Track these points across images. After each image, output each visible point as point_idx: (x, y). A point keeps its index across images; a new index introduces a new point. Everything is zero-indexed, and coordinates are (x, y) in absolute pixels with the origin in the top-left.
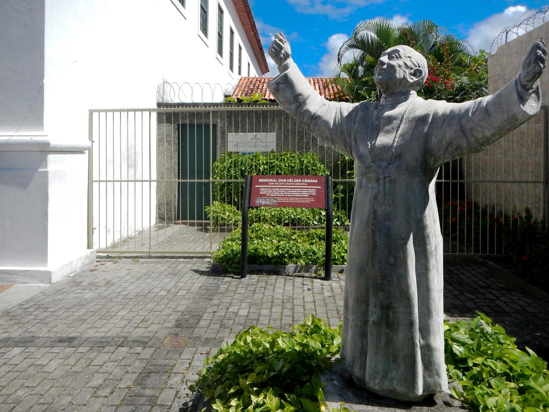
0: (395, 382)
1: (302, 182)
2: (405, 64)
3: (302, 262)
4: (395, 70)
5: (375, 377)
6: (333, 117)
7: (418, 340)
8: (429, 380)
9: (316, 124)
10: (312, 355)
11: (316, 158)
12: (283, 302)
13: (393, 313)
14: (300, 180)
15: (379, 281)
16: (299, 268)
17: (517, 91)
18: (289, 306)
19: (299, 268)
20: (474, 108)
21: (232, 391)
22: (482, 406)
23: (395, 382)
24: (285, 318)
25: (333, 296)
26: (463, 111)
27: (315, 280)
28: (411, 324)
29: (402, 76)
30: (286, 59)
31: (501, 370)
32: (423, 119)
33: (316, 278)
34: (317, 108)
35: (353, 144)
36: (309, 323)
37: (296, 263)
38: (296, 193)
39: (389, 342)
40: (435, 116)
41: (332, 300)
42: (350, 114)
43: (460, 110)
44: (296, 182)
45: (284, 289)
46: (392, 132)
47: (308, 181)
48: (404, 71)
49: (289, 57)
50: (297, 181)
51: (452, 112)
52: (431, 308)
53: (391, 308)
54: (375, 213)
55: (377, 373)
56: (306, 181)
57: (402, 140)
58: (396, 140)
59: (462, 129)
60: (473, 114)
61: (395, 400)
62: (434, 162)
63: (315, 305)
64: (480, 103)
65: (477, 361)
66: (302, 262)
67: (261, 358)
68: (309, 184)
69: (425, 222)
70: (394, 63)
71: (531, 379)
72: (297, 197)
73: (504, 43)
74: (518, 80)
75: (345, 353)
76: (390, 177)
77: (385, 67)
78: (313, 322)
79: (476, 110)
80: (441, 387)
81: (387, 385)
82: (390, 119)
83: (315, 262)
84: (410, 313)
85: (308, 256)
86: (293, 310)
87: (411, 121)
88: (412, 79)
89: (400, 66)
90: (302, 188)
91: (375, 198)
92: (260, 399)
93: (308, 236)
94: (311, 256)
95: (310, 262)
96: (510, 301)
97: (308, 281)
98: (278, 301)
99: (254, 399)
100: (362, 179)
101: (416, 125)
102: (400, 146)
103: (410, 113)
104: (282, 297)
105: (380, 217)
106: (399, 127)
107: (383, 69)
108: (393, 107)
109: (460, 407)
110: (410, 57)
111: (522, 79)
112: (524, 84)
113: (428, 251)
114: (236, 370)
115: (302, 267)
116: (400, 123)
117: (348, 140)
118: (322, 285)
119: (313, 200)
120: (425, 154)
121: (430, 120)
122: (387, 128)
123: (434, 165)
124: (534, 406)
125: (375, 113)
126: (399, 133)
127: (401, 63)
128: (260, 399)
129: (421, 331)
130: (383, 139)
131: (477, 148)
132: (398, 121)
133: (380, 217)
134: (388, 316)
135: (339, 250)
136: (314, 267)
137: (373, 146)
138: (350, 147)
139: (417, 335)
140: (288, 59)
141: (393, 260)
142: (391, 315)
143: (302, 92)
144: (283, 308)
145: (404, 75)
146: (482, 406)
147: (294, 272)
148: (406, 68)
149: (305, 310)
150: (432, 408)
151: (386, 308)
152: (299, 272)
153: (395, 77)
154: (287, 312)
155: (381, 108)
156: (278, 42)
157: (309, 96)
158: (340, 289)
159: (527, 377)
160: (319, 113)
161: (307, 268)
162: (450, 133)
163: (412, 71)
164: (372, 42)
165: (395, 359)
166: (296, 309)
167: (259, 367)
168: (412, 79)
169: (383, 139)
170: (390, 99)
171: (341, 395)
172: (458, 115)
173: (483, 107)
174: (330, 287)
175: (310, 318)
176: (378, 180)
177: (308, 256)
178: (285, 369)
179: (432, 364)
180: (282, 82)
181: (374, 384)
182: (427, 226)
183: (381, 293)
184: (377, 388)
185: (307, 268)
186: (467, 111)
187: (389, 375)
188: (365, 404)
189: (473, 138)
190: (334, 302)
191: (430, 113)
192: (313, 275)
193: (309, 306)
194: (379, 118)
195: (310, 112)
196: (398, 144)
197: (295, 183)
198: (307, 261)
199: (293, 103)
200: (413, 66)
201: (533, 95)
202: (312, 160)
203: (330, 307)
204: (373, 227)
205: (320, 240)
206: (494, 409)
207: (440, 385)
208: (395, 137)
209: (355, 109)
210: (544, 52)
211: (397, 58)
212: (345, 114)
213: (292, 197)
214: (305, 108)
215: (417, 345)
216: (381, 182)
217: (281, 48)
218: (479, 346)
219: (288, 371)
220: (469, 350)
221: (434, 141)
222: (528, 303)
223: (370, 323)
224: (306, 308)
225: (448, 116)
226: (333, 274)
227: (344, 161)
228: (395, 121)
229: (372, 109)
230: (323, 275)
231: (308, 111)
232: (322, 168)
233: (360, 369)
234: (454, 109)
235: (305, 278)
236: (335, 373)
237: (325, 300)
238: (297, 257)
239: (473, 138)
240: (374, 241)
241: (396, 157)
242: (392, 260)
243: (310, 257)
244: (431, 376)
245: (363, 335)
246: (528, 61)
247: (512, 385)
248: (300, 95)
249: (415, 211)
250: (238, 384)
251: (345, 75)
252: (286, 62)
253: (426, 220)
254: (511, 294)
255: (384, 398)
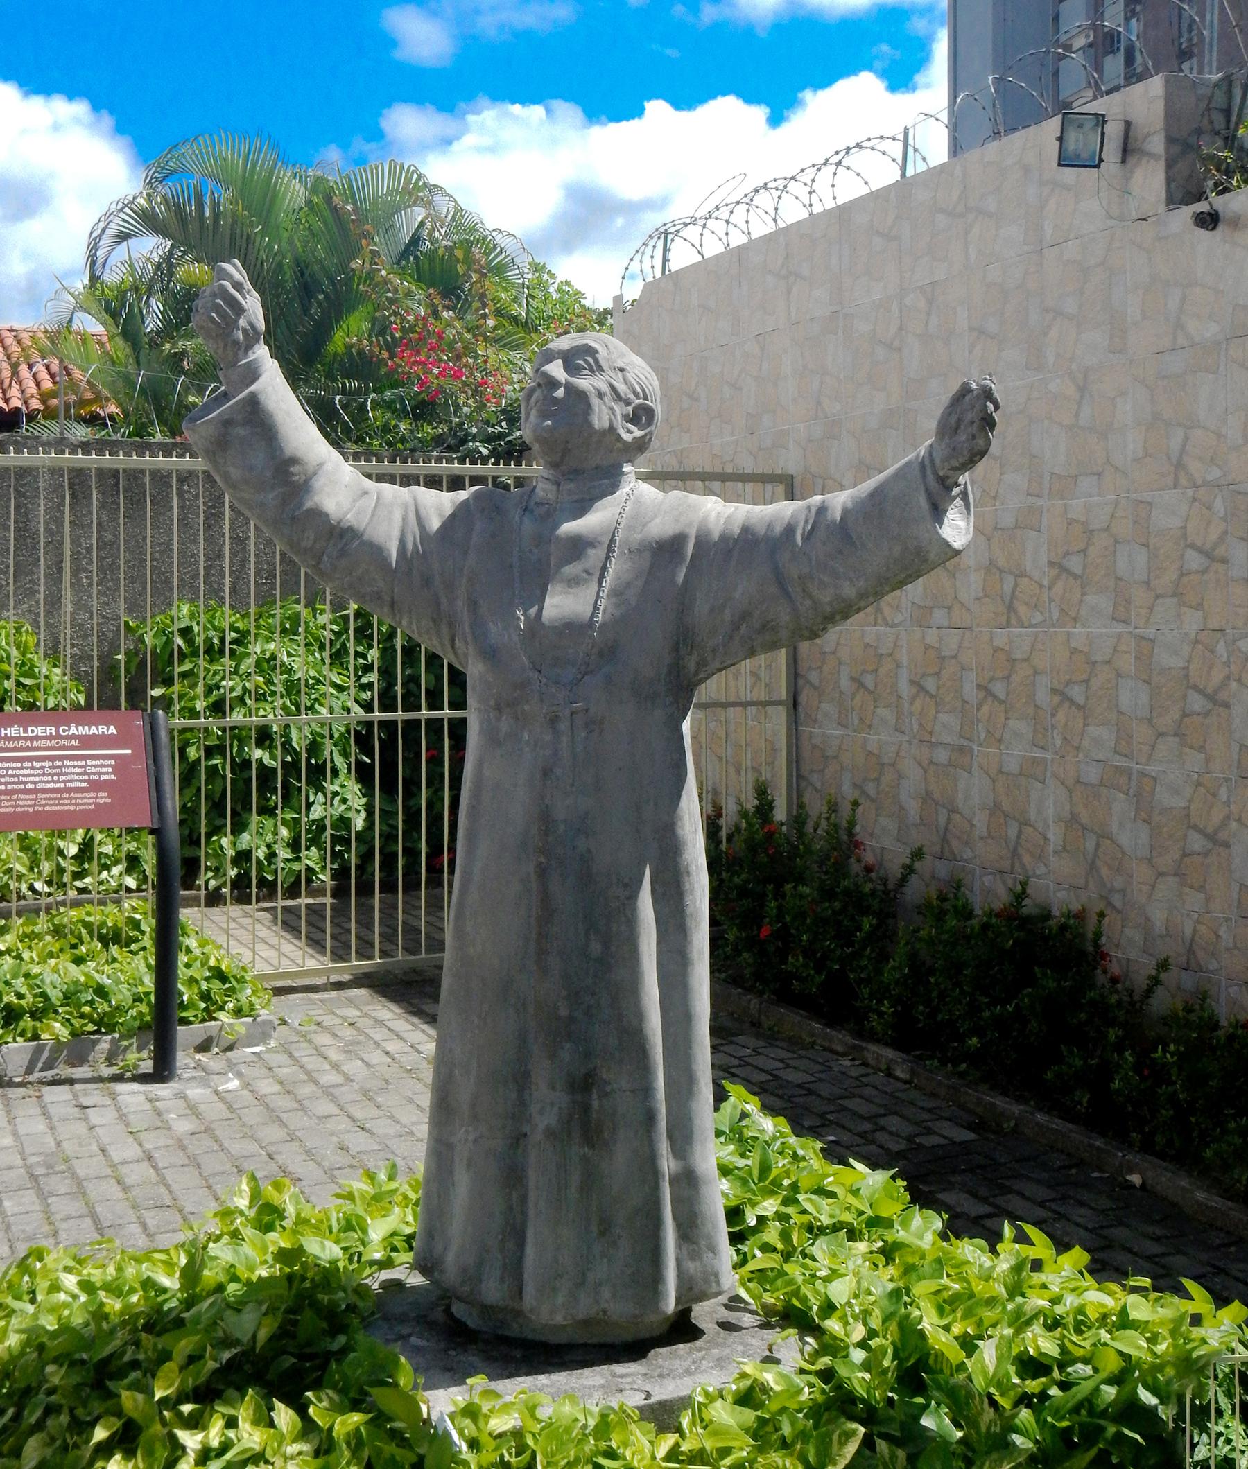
0: (606, 1293)
1: (58, 736)
2: (613, 388)
3: (58, 1029)
4: (589, 406)
5: (554, 1289)
6: (396, 533)
7: (667, 1164)
8: (691, 1266)
9: (343, 553)
10: (328, 1277)
11: (32, 641)
12: (34, 1178)
13: (600, 1098)
14: (51, 730)
15: (564, 1012)
16: (46, 1054)
17: (927, 490)
18: (61, 1185)
19: (46, 1054)
20: (806, 522)
21: (100, 1434)
22: (815, 1308)
23: (606, 1293)
24: (64, 1225)
25: (208, 1130)
26: (778, 529)
27: (121, 1087)
28: (650, 1118)
29: (606, 425)
30: (249, 347)
31: (831, 1216)
32: (667, 550)
33: (118, 1078)
34: (346, 504)
35: (465, 617)
36: (243, 1203)
37: (36, 1037)
38: (37, 775)
39: (591, 1180)
40: (702, 542)
41: (207, 1142)
42: (451, 523)
43: (770, 526)
44: (37, 738)
45: (15, 1134)
46: (586, 581)
47: (84, 730)
48: (612, 409)
49: (258, 341)
50: (39, 731)
51: (746, 529)
52: (695, 1067)
53: (592, 1084)
54: (545, 818)
55: (561, 1276)
56: (73, 730)
57: (617, 606)
58: (602, 604)
59: (780, 580)
60: (807, 537)
61: (602, 1346)
62: (698, 664)
63: (155, 1167)
64: (822, 510)
65: (765, 1209)
66: (58, 1029)
67: (158, 1322)
68: (87, 742)
69: (680, 832)
70: (584, 383)
71: (897, 1226)
72: (44, 791)
73: (658, 275)
74: (927, 462)
75: (439, 1248)
76: (587, 711)
77: (560, 393)
78: (255, 1195)
79: (813, 529)
80: (718, 1283)
81: (585, 1307)
82: (578, 546)
83: (105, 1024)
84: (646, 1091)
85: (79, 1006)
86: (84, 1194)
87: (636, 551)
88: (629, 432)
89: (600, 395)
90: (61, 758)
91: (546, 773)
92: (215, 1434)
93: (58, 932)
94: (91, 1003)
95: (91, 1027)
96: (736, 1062)
97: (93, 1095)
98: (13, 1174)
99: (191, 1440)
100: (498, 720)
101: (652, 567)
102: (616, 623)
103: (630, 528)
104: (19, 1162)
105: (562, 828)
106: (604, 569)
107: (556, 401)
108: (581, 509)
109: (760, 1327)
110: (622, 370)
111: (938, 462)
112: (941, 473)
113: (689, 911)
114: (76, 1379)
115: (58, 1045)
116: (608, 558)
117: (444, 600)
118: (151, 1101)
119: (104, 798)
120: (677, 643)
121: (690, 550)
122: (570, 570)
123: (696, 673)
124: (932, 1277)
125: (529, 526)
126: (608, 583)
127: (605, 388)
128: (215, 1434)
129: (670, 1136)
130: (562, 604)
131: (815, 628)
132: (601, 553)
133: (562, 828)
134: (586, 1108)
135: (190, 972)
136: (105, 1043)
137: (536, 622)
138: (451, 625)
139: (664, 1147)
140: (257, 346)
141: (599, 947)
142: (595, 1104)
143: (299, 454)
144: (43, 1196)
145: (610, 420)
146: (815, 1308)
147: (29, 1070)
148: (615, 401)
149: (126, 1189)
150: (698, 1343)
151: (583, 1085)
152: (48, 1066)
153: (590, 425)
154: (61, 1207)
155: (542, 510)
156: (232, 291)
157: (321, 465)
158: (221, 1105)
159: (887, 1223)
160: (351, 519)
161: (77, 1049)
162: (744, 587)
163: (630, 409)
164: (216, 215)
165: (605, 1227)
166: (95, 1191)
167: (183, 1343)
168: (629, 432)
169: (562, 604)
170: (572, 486)
171: (448, 1369)
172: (767, 538)
173: (833, 522)
174: (181, 1103)
175: (244, 1187)
176: (553, 721)
177: (79, 1006)
178: (263, 1335)
179: (699, 1221)
180: (239, 417)
181: (549, 1311)
182: (685, 843)
183: (568, 1045)
184: (559, 1319)
185: (77, 1049)
186: (790, 530)
187: (591, 1276)
188: (527, 1374)
189: (808, 603)
190: (216, 1147)
191: (687, 530)
192: (107, 1072)
193: (137, 1173)
194: (545, 537)
195: (327, 515)
196: (608, 616)
197: (31, 739)
198: (77, 1023)
199: (273, 488)
200: (632, 396)
201: (958, 502)
202: (15, 652)
203: (212, 1164)
204: (543, 860)
205: (106, 945)
206: (853, 1301)
207: (716, 1275)
208: (598, 597)
209: (462, 511)
210: (997, 407)
211: (592, 371)
212: (435, 524)
213: (26, 792)
214: (309, 504)
215: (664, 1177)
216: (563, 726)
217: (239, 310)
218: (765, 1168)
219: (272, 1339)
220: (744, 1182)
221: (701, 607)
222: (782, 1061)
223: (537, 1136)
224: (129, 1181)
225: (736, 541)
226: (184, 1058)
227: (137, 653)
228: (591, 552)
229: (515, 515)
230: (147, 1066)
231: (318, 514)
232: (55, 679)
233: (502, 1279)
234: (753, 521)
235: (78, 1087)
236: (403, 1319)
237: (183, 1148)
238: (34, 1015)
239: (808, 603)
240: (545, 897)
241: (601, 654)
242: (596, 948)
243: (86, 1009)
244: (695, 1256)
245: (513, 1177)
246: (954, 418)
247: (862, 1246)
248: (294, 461)
249: (656, 804)
250: (119, 1413)
251: (91, 324)
252: (251, 357)
253: (683, 825)
254: (732, 1042)
255: (570, 1347)
